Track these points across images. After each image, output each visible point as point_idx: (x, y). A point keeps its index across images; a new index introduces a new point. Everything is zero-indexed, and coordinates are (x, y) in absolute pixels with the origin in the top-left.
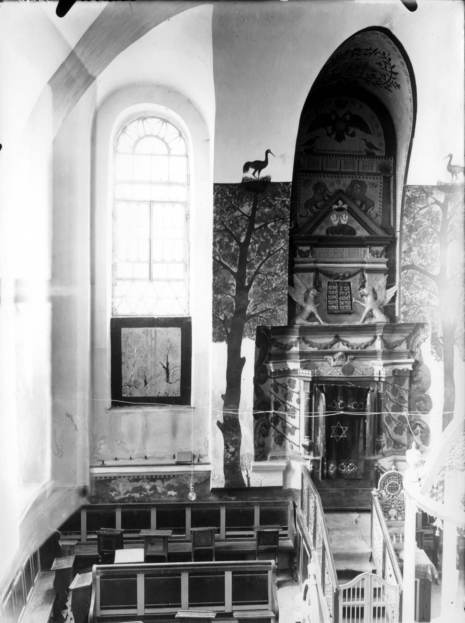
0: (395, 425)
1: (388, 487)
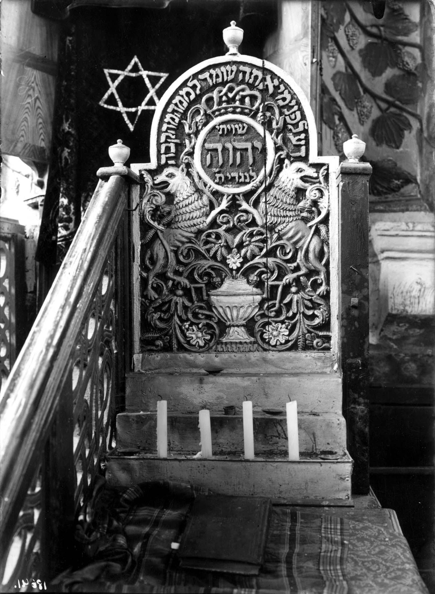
0: (375, 113)
1: (205, 151)
